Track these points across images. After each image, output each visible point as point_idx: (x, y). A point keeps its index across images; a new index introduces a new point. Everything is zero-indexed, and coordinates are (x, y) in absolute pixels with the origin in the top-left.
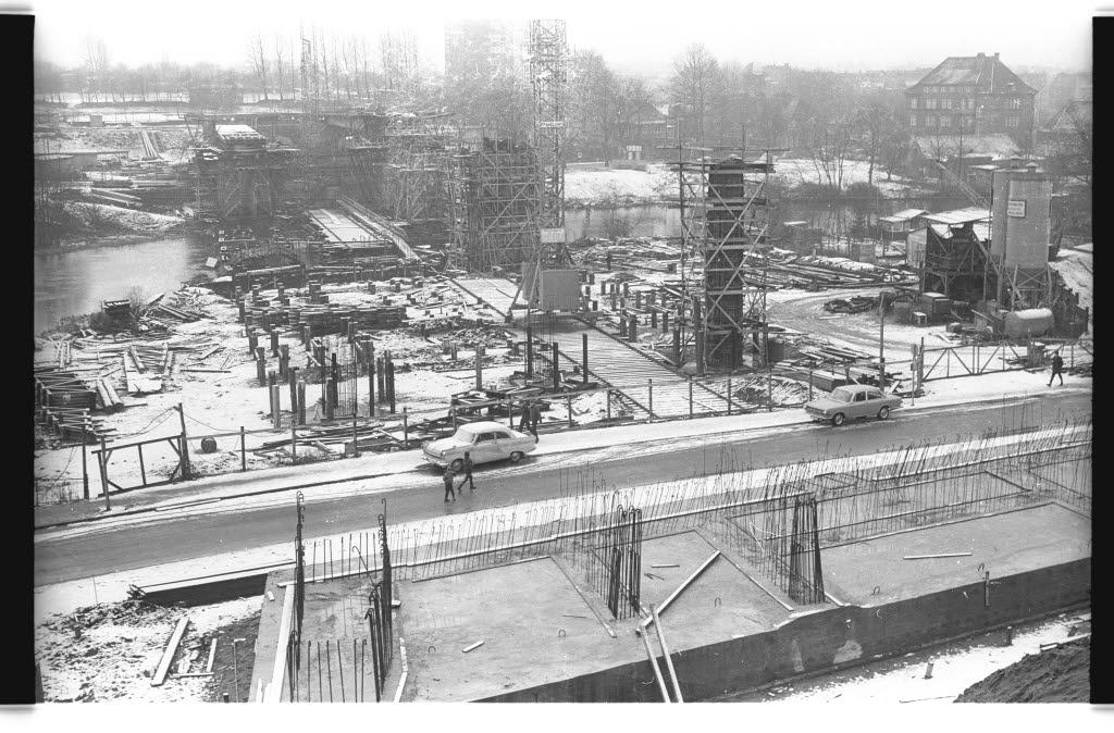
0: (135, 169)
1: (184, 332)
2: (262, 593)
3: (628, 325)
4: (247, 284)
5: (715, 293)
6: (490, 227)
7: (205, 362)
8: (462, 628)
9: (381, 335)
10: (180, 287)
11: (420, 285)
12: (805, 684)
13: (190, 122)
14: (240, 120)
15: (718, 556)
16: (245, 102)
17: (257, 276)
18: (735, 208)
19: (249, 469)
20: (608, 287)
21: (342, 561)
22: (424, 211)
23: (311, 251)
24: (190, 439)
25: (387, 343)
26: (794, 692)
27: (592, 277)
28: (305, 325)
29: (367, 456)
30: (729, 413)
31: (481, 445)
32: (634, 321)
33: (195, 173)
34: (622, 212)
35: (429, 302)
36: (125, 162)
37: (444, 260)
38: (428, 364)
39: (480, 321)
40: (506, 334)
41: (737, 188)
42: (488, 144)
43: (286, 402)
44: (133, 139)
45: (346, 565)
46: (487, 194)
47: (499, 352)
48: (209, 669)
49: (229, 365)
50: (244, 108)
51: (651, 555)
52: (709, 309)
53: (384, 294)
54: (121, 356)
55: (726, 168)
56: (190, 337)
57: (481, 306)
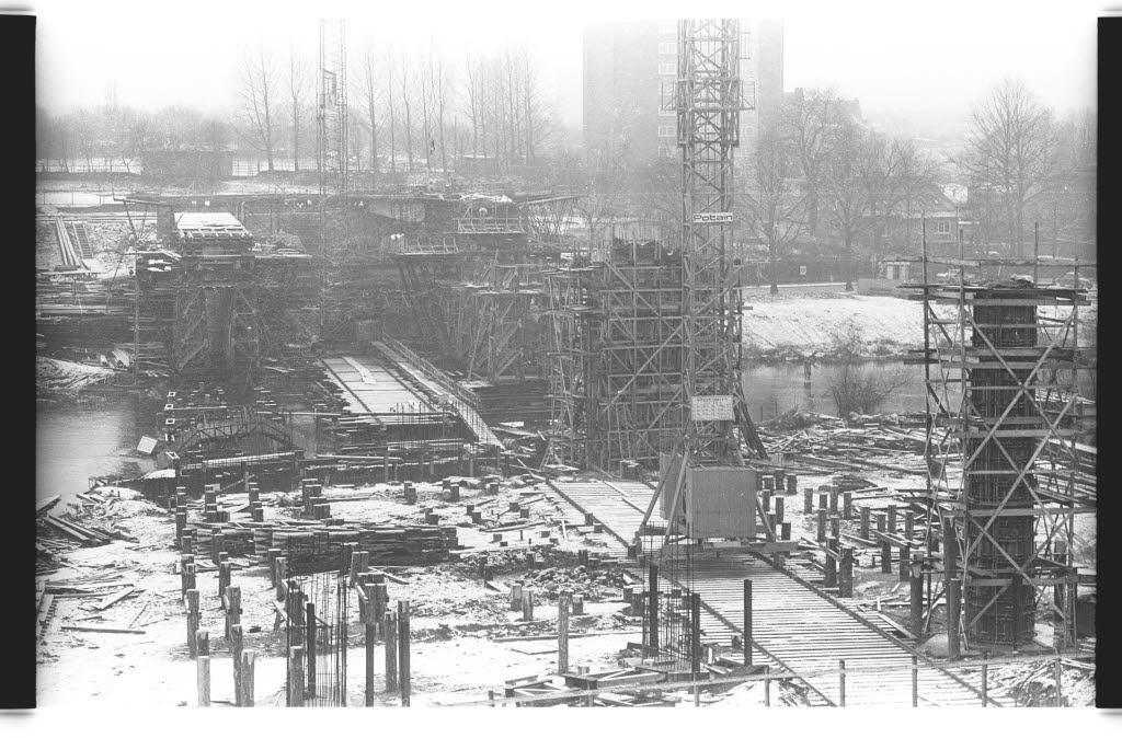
4: (195, 483)
5: (982, 513)
9: (409, 575)
11: (494, 491)
17: (220, 470)
22: (518, 363)
23: (321, 431)
28: (279, 554)
32: (849, 558)
33: (134, 294)
35: (504, 520)
37: (542, 446)
38: (482, 628)
39: (583, 554)
46: (618, 335)
47: (607, 609)
49: (143, 620)
50: (232, 183)
52: (973, 540)
53: (430, 504)
56: (87, 571)
57: (591, 529)
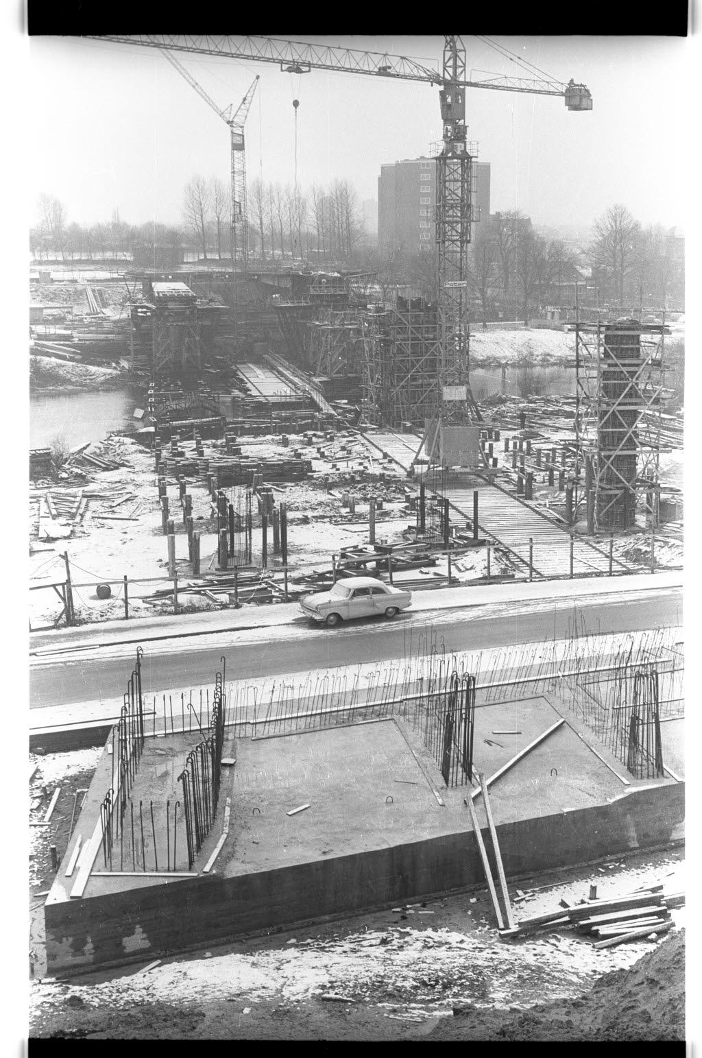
0: (78, 324)
1: (102, 480)
2: (103, 744)
3: (524, 482)
4: (166, 435)
5: (608, 453)
6: (403, 383)
7: (115, 509)
8: (290, 790)
9: (286, 487)
10: (105, 436)
11: (332, 439)
12: (637, 861)
13: (128, 280)
14: (176, 278)
15: (562, 723)
16: (185, 261)
18: (632, 369)
19: (132, 617)
20: (511, 444)
21: (271, 703)
24: (74, 586)
25: (291, 495)
26: (625, 869)
27: (498, 434)
28: (212, 476)
29: (247, 608)
30: (611, 574)
31: (357, 599)
32: (531, 478)
34: (537, 370)
35: (338, 456)
36: (70, 317)
37: (358, 414)
38: (327, 517)
40: (406, 489)
41: (632, 349)
42: (402, 302)
43: (183, 550)
44: (78, 296)
45: (187, 720)
46: (400, 351)
47: (396, 506)
48: (46, 819)
51: (486, 722)
52: (602, 468)
54: (38, 502)
55: (621, 329)
56: (106, 485)
57: (386, 461)
